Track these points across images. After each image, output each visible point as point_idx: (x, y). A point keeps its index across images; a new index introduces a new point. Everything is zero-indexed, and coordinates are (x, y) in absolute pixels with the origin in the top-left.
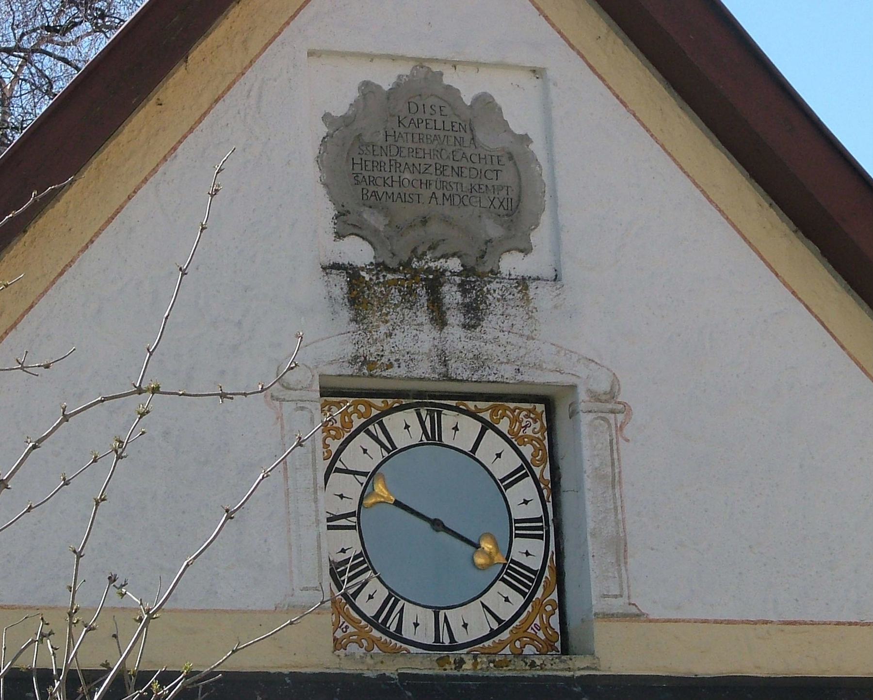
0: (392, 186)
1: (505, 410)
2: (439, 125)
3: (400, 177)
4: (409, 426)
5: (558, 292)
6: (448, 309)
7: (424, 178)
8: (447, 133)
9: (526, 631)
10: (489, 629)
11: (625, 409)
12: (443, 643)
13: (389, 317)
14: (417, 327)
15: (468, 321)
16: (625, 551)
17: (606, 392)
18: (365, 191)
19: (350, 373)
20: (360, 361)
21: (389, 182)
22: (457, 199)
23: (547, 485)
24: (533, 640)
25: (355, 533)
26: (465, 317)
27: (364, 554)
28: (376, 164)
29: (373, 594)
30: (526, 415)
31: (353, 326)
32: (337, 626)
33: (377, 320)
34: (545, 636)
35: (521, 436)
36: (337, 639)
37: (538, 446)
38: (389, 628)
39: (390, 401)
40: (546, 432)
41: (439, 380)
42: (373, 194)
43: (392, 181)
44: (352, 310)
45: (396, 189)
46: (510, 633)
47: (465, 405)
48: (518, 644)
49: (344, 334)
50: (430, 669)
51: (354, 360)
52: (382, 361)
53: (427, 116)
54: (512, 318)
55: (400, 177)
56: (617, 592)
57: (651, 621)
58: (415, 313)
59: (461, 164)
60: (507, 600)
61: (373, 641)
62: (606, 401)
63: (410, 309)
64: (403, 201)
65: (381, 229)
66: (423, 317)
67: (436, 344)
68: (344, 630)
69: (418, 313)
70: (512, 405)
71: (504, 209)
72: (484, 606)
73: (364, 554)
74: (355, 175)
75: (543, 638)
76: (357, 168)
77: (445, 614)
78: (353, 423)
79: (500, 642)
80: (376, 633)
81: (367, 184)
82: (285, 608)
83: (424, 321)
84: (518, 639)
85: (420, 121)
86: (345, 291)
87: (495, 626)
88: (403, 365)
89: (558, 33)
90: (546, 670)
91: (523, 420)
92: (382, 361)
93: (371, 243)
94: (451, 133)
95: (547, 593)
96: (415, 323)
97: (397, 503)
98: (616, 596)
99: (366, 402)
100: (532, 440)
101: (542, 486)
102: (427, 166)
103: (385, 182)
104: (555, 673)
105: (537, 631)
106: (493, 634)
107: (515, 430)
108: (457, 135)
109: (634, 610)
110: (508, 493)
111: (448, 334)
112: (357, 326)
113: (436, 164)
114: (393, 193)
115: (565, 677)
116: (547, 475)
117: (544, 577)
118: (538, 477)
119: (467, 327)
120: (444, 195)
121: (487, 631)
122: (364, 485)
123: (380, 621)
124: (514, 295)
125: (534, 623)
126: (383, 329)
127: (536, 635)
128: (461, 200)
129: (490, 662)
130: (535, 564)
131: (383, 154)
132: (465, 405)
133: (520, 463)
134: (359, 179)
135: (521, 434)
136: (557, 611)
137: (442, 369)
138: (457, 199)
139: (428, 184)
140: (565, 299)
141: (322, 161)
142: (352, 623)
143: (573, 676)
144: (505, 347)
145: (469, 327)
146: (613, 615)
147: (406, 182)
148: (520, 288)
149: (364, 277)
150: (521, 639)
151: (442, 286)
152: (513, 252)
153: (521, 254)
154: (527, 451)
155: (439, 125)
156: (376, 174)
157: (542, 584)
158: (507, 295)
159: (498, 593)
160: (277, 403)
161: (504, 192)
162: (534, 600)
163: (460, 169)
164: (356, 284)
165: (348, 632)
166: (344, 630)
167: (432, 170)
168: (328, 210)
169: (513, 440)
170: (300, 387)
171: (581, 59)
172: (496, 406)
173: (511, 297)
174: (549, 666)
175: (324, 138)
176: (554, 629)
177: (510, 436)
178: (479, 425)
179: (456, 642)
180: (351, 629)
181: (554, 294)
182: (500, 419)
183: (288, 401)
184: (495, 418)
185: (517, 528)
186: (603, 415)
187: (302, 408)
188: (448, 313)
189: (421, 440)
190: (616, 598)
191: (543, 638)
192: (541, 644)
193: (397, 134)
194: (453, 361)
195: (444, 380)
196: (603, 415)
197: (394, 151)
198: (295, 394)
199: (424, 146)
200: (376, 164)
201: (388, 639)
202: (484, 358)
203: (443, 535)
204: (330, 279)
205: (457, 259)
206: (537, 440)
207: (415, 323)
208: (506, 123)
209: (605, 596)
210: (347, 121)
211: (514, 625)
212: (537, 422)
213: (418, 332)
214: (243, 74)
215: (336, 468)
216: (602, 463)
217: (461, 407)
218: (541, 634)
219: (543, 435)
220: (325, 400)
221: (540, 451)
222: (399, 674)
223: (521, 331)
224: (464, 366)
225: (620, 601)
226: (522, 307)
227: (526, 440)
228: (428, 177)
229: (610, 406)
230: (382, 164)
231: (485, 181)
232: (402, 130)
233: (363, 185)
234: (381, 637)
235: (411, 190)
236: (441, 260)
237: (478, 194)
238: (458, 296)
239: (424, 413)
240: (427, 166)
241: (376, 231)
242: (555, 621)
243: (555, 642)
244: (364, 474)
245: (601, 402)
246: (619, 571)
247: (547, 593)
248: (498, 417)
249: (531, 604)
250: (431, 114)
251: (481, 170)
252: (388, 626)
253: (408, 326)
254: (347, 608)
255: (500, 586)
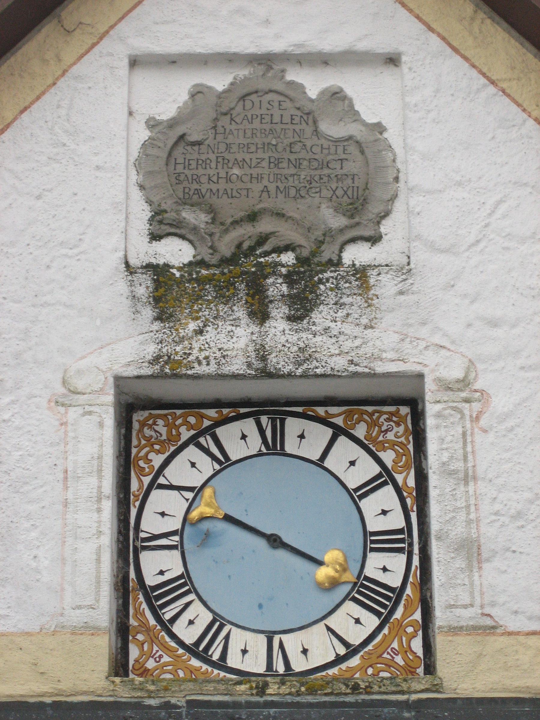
0: (218, 183)
1: (362, 414)
2: (277, 119)
3: (227, 173)
4: (246, 436)
5: (404, 277)
6: (271, 302)
7: (255, 172)
8: (284, 126)
9: (380, 656)
10: (335, 655)
11: (483, 397)
12: (276, 671)
13: (201, 314)
14: (232, 322)
15: (293, 312)
16: (479, 555)
17: (459, 379)
18: (187, 190)
19: (150, 373)
20: (163, 361)
21: (215, 179)
22: (293, 192)
23: (411, 494)
24: (390, 666)
25: (176, 554)
26: (290, 309)
27: (186, 575)
28: (200, 162)
29: (194, 619)
30: (387, 418)
31: (157, 325)
32: (149, 655)
33: (186, 317)
34: (404, 661)
35: (381, 442)
36: (149, 670)
37: (401, 451)
38: (211, 656)
39: (225, 411)
40: (411, 436)
41: (255, 377)
42: (196, 192)
43: (218, 178)
44: (156, 308)
45: (222, 185)
46: (360, 659)
47: (312, 411)
48: (370, 671)
49: (146, 333)
50: (226, 694)
51: (156, 359)
52: (189, 359)
53: (264, 111)
54: (347, 307)
55: (227, 173)
56: (467, 601)
57: (510, 634)
58: (231, 308)
59: (301, 156)
60: (357, 621)
61: (191, 672)
62: (459, 390)
63: (225, 304)
64: (230, 196)
65: (202, 226)
66: (240, 312)
67: (254, 338)
68: (158, 659)
69: (235, 308)
70: (370, 409)
71: (349, 198)
72: (329, 629)
73: (186, 575)
74: (176, 175)
75: (402, 663)
76: (180, 168)
77: (280, 638)
78: (181, 436)
79: (349, 669)
80: (195, 663)
81: (189, 183)
82: (52, 629)
83: (241, 315)
84: (371, 666)
85: (255, 117)
86: (151, 289)
87: (342, 651)
88: (213, 362)
89: (416, 17)
90: (373, 693)
91: (383, 425)
92: (189, 359)
93: (191, 242)
94: (290, 126)
95: (407, 612)
96: (231, 318)
97: (228, 518)
98: (465, 607)
99: (198, 413)
100: (394, 445)
101: (405, 494)
102: (259, 161)
103: (209, 179)
104: (384, 697)
105: (394, 656)
106: (339, 660)
107: (374, 435)
108: (297, 127)
109: (489, 622)
110: (364, 504)
111: (269, 327)
112: (162, 325)
113: (270, 157)
114: (218, 190)
115: (397, 701)
116: (411, 482)
117: (405, 595)
118: (400, 484)
119: (292, 318)
120: (277, 187)
121: (331, 657)
122: (190, 501)
123: (201, 649)
124: (350, 283)
125: (392, 646)
126: (192, 326)
127: (393, 660)
128: (298, 191)
129: (302, 684)
130: (395, 581)
131: (210, 151)
132: (312, 411)
133: (377, 469)
134: (180, 179)
135: (381, 438)
136: (420, 633)
137: (258, 364)
138: (293, 192)
139: (259, 178)
140: (412, 284)
141: (140, 164)
142: (169, 653)
143: (408, 700)
144: (337, 338)
145: (295, 319)
146: (461, 627)
147: (234, 177)
148: (358, 276)
149: (174, 274)
150: (373, 666)
151: (265, 279)
152: (359, 242)
153: (368, 243)
154: (388, 457)
155: (277, 119)
156: (201, 171)
157: (403, 602)
158: (342, 283)
159: (348, 614)
160: (62, 409)
161: (349, 181)
162: (391, 621)
163: (298, 160)
164: (163, 282)
165: (161, 662)
166: (158, 659)
167: (265, 164)
168: (143, 212)
169: (371, 446)
170: (88, 391)
171: (442, 42)
172: (351, 411)
173: (347, 285)
174: (376, 688)
175: (145, 141)
176: (415, 653)
177: (366, 442)
178: (329, 432)
179: (294, 671)
180: (166, 659)
181: (400, 279)
182: (355, 424)
183: (75, 406)
184: (349, 423)
185: (372, 542)
186: (455, 404)
187: (90, 413)
188: (271, 306)
189: (260, 450)
190: (466, 608)
191: (402, 663)
192: (399, 671)
193: (227, 131)
194: (274, 355)
195: (262, 376)
196: (455, 404)
197: (222, 147)
198: (82, 399)
199: (256, 140)
200: (200, 162)
201: (210, 669)
202: (312, 350)
203: (282, 554)
204: (135, 279)
205: (291, 252)
206: (399, 444)
207: (231, 318)
208: (357, 113)
209: (451, 606)
210: (172, 123)
211: (366, 649)
212: (401, 425)
213: (234, 328)
214: (54, 84)
215: (159, 484)
216: (452, 457)
217: (309, 413)
218: (399, 660)
219: (407, 439)
220: (150, 413)
221: (404, 457)
222: (188, 702)
223: (358, 321)
224: (287, 360)
225: (467, 613)
226: (360, 295)
227: (386, 445)
228: (259, 171)
229: (464, 395)
230: (208, 162)
231: (326, 171)
232: (234, 126)
233: (185, 184)
234: (201, 667)
235: (240, 185)
236: (273, 255)
237: (318, 185)
238: (284, 289)
239: (264, 419)
240: (259, 161)
241: (195, 229)
242: (417, 645)
243: (416, 668)
244: (161, 487)
245: (452, 390)
246: (470, 577)
247: (407, 612)
248: (354, 422)
249: (388, 625)
250: (268, 109)
251: (323, 160)
252: (210, 653)
253: (223, 323)
254: (163, 636)
255: (351, 607)
